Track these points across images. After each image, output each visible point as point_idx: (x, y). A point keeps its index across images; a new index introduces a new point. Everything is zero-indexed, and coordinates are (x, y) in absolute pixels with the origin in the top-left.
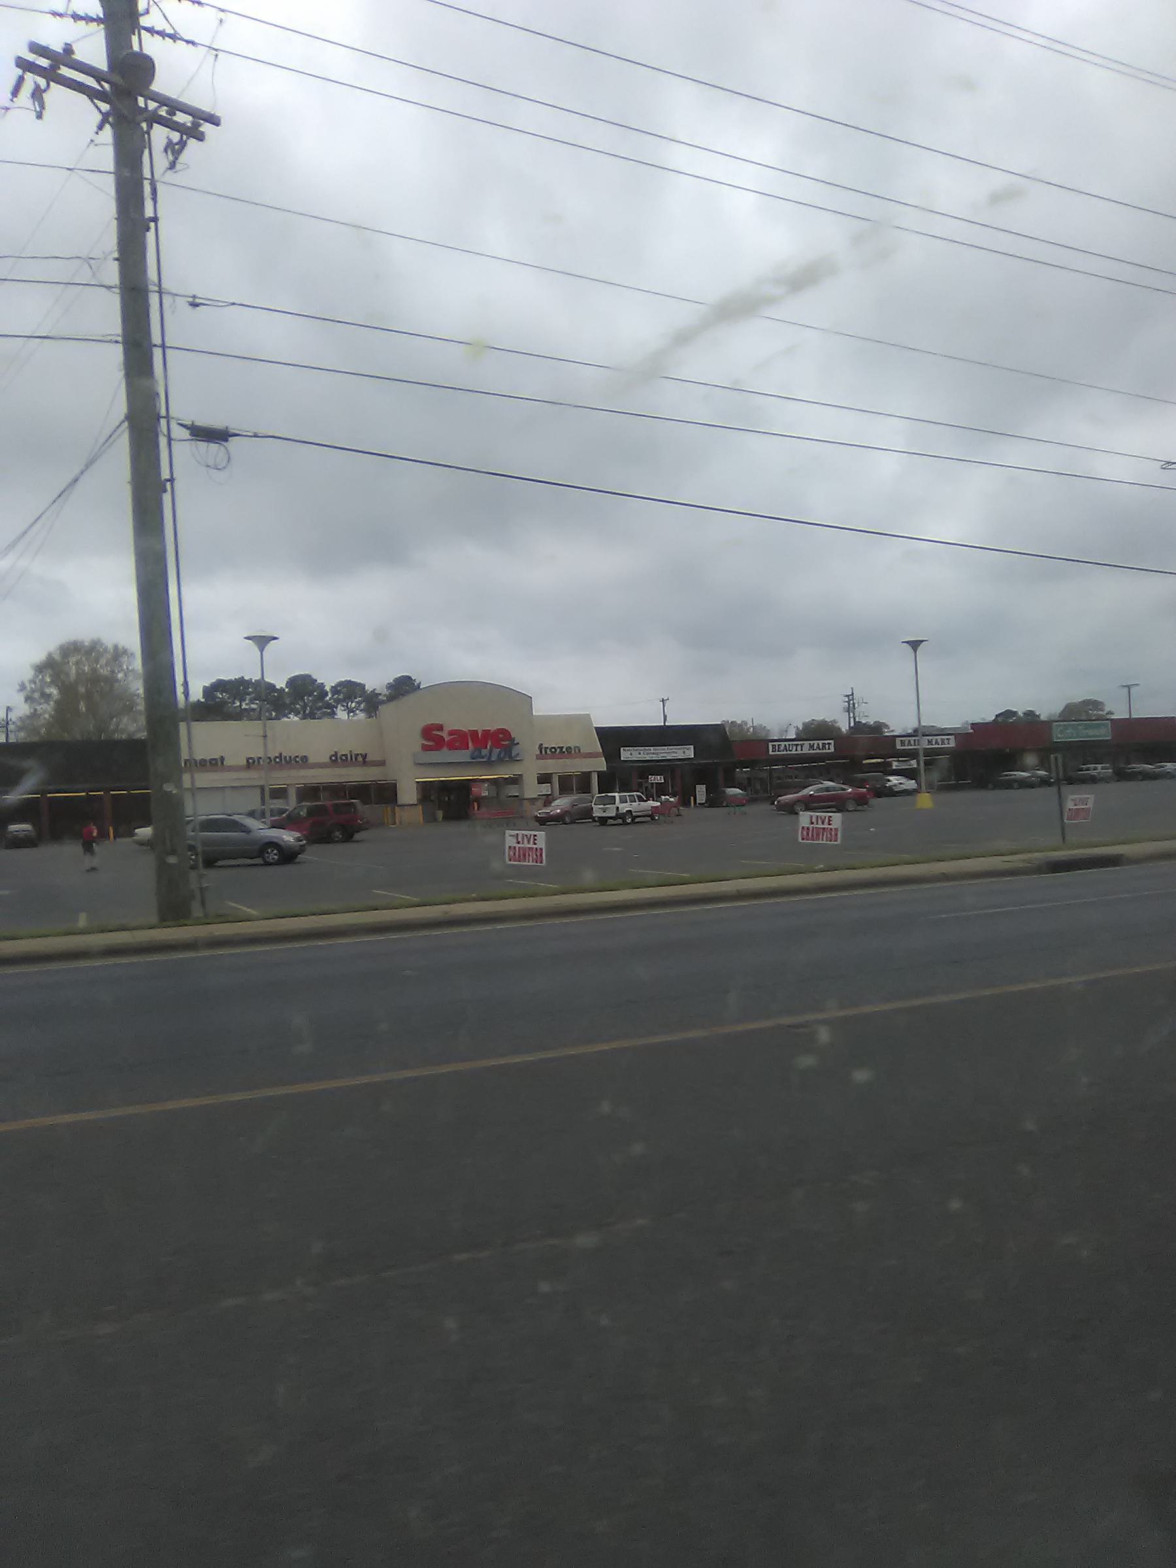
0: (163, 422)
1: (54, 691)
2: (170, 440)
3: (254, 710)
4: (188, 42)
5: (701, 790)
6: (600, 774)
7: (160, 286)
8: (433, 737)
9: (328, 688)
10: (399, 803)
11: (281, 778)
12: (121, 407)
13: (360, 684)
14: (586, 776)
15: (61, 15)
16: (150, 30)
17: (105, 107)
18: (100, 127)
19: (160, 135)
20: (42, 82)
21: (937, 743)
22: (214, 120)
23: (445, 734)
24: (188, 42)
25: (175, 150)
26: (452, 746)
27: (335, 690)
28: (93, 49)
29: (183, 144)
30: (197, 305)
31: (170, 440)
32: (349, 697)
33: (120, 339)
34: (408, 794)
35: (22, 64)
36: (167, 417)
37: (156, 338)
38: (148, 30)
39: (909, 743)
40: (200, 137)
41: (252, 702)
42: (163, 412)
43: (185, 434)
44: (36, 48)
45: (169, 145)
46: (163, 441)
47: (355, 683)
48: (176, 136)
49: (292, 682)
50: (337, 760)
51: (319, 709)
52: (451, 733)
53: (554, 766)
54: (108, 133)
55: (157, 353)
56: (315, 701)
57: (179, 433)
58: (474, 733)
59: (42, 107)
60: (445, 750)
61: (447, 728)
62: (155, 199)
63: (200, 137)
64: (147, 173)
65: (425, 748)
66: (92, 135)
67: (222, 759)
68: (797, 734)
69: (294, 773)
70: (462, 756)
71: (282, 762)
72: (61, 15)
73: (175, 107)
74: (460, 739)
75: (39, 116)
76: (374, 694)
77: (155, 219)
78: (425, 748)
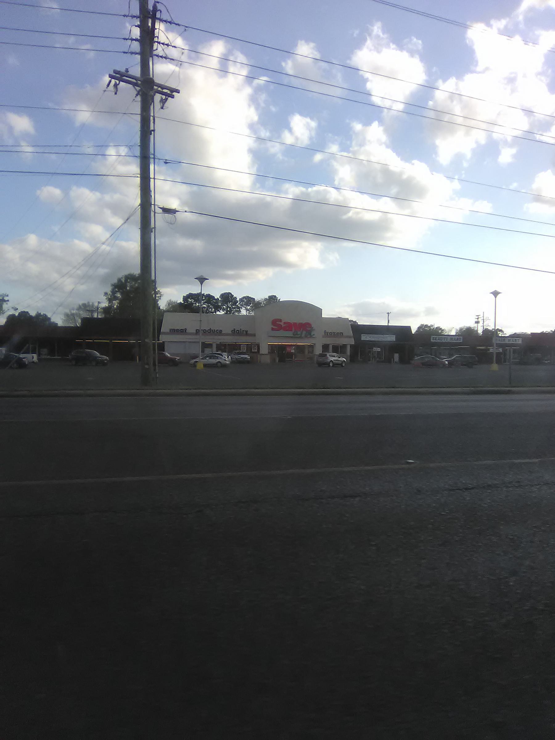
0: (153, 206)
1: (118, 295)
2: (155, 213)
3: (204, 307)
4: (173, 47)
5: (396, 356)
6: (351, 346)
7: (154, 155)
8: (277, 325)
9: (238, 299)
10: (260, 353)
11: (208, 339)
12: (139, 201)
13: (252, 298)
14: (344, 346)
15: (126, 53)
16: (157, 56)
17: (138, 88)
18: (137, 95)
19: (158, 97)
20: (118, 82)
21: (499, 341)
22: (178, 91)
23: (282, 323)
24: (173, 47)
25: (163, 102)
26: (285, 329)
27: (241, 300)
28: (136, 71)
29: (166, 99)
30: (167, 163)
31: (155, 213)
32: (247, 304)
33: (139, 176)
34: (264, 350)
35: (111, 77)
36: (154, 205)
37: (152, 176)
38: (155, 55)
39: (437, 339)
40: (173, 97)
41: (204, 304)
42: (153, 203)
43: (161, 211)
44: (115, 72)
45: (162, 99)
46: (152, 214)
47: (250, 297)
48: (164, 97)
49: (222, 296)
50: (235, 332)
51: (234, 308)
52: (285, 323)
53: (329, 341)
54: (139, 98)
55: (152, 180)
56: (232, 305)
57: (159, 210)
58: (295, 324)
59: (117, 90)
60: (282, 330)
61: (283, 321)
62: (154, 123)
63: (173, 97)
64: (152, 114)
65: (273, 329)
66: (134, 98)
67: (186, 329)
68: (457, 333)
69: (216, 337)
70: (290, 334)
71: (211, 332)
72: (126, 53)
73: (163, 87)
74: (289, 327)
75: (116, 94)
76: (259, 303)
77: (154, 131)
78: (273, 329)
